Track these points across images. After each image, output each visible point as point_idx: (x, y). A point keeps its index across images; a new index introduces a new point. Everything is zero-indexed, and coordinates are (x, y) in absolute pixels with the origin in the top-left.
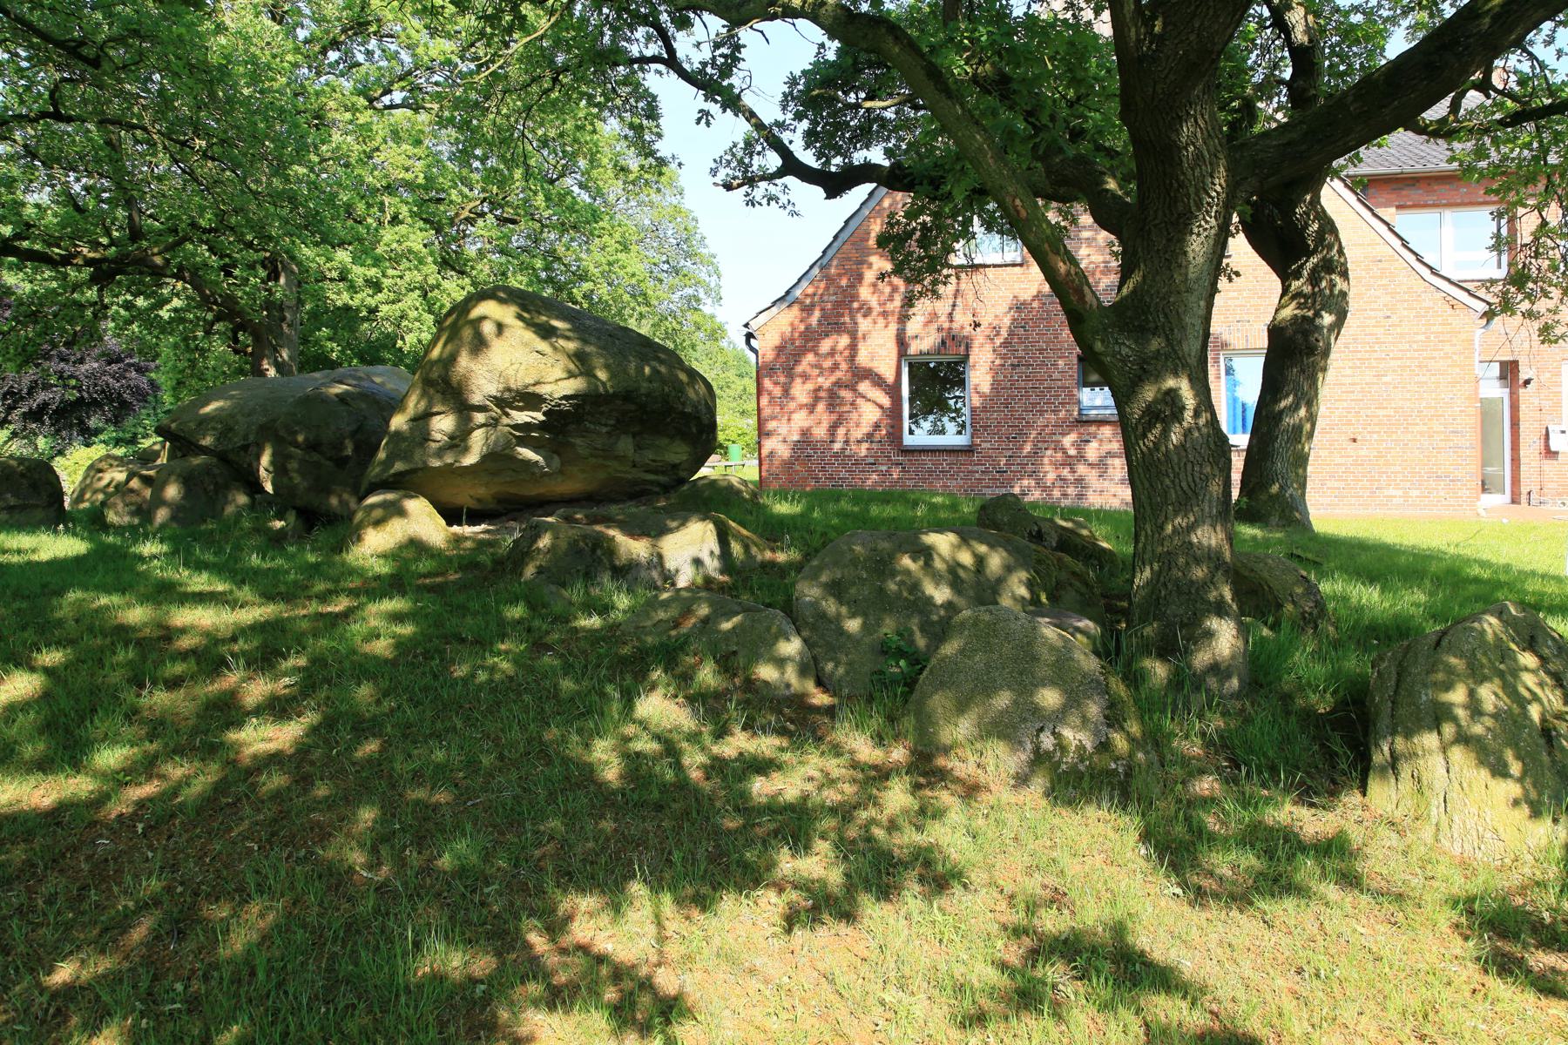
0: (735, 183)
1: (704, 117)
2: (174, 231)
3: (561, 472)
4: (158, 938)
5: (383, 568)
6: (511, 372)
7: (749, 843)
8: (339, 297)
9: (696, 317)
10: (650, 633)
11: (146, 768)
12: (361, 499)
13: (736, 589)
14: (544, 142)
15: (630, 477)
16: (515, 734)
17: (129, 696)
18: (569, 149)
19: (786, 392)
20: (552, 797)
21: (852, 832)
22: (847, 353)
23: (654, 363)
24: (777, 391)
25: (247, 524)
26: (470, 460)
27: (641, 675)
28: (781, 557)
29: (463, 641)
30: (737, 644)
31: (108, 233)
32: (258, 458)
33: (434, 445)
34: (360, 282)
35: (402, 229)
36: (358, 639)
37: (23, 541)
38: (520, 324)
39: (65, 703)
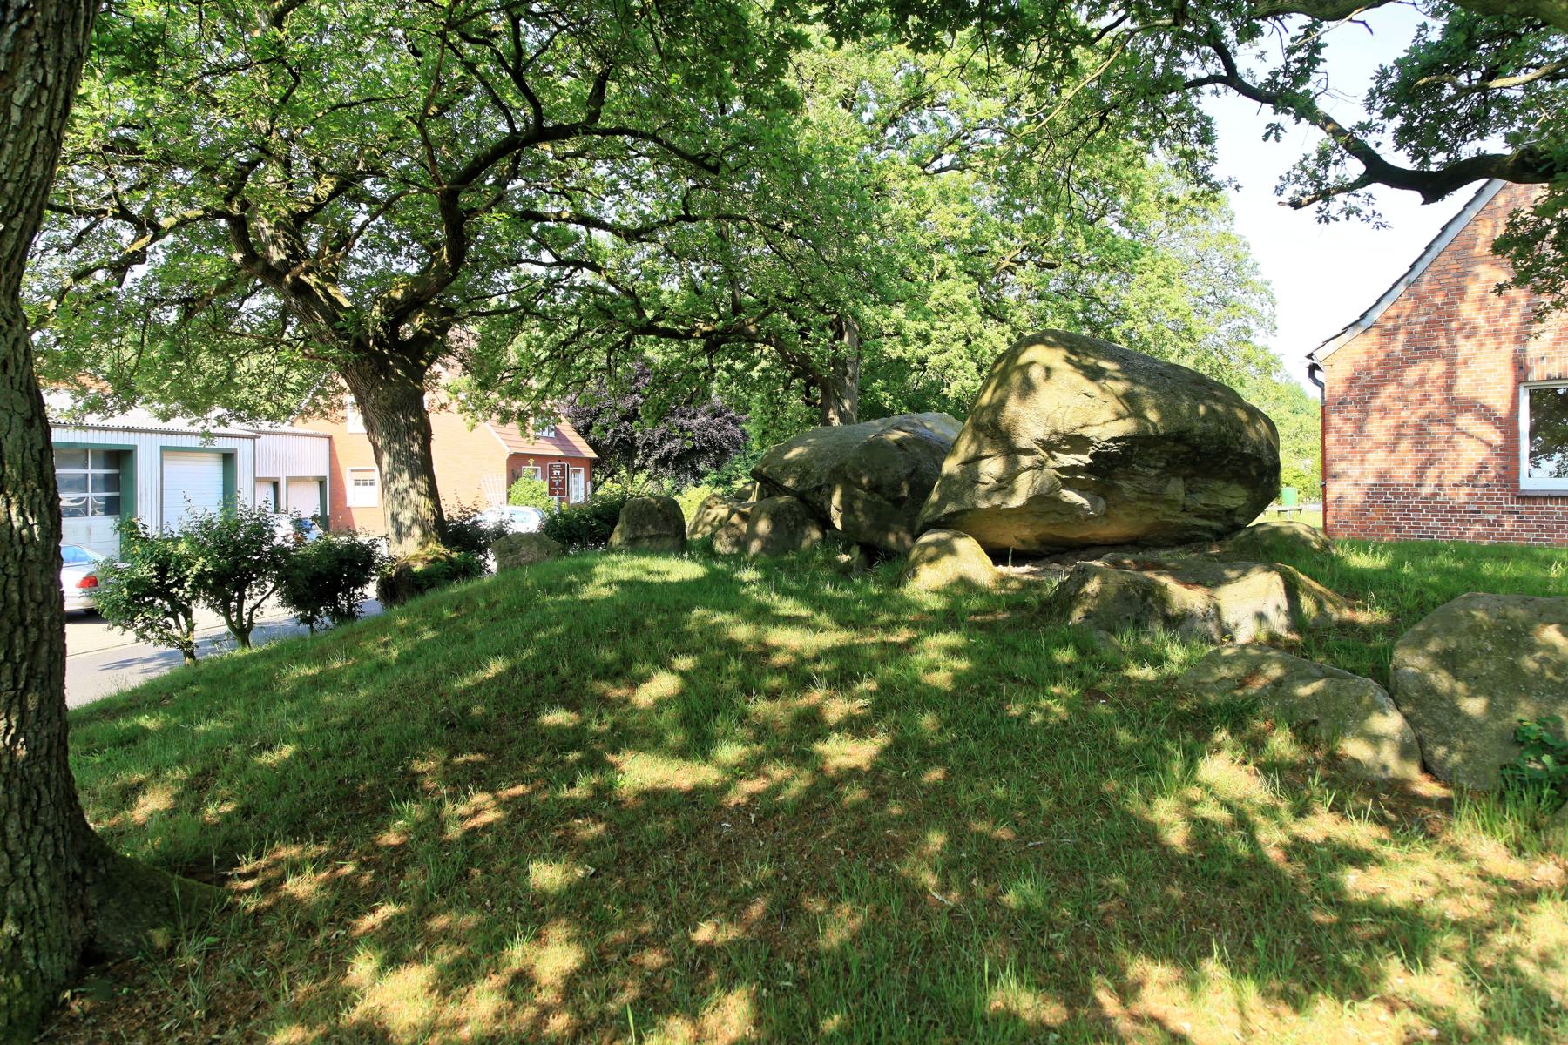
0: (1305, 200)
1: (1274, 131)
2: (765, 303)
3: (1106, 515)
4: (770, 918)
5: (937, 604)
6: (1058, 415)
7: (1348, 945)
8: (892, 349)
9: (1246, 350)
10: (1212, 691)
11: (753, 766)
12: (915, 537)
13: (1309, 649)
14: (1085, 184)
15: (1179, 521)
16: (1072, 780)
17: (739, 700)
18: (1109, 187)
19: (1359, 429)
20: (1114, 851)
21: (1486, 959)
22: (1441, 382)
23: (1208, 402)
24: (1348, 428)
25: (820, 557)
26: (1016, 501)
27: (1203, 735)
28: (1363, 617)
29: (1015, 680)
30: (1318, 713)
31: (717, 310)
32: (830, 497)
33: (982, 488)
34: (912, 335)
35: (949, 283)
36: (920, 670)
37: (659, 564)
38: (1069, 367)
39: (696, 703)
